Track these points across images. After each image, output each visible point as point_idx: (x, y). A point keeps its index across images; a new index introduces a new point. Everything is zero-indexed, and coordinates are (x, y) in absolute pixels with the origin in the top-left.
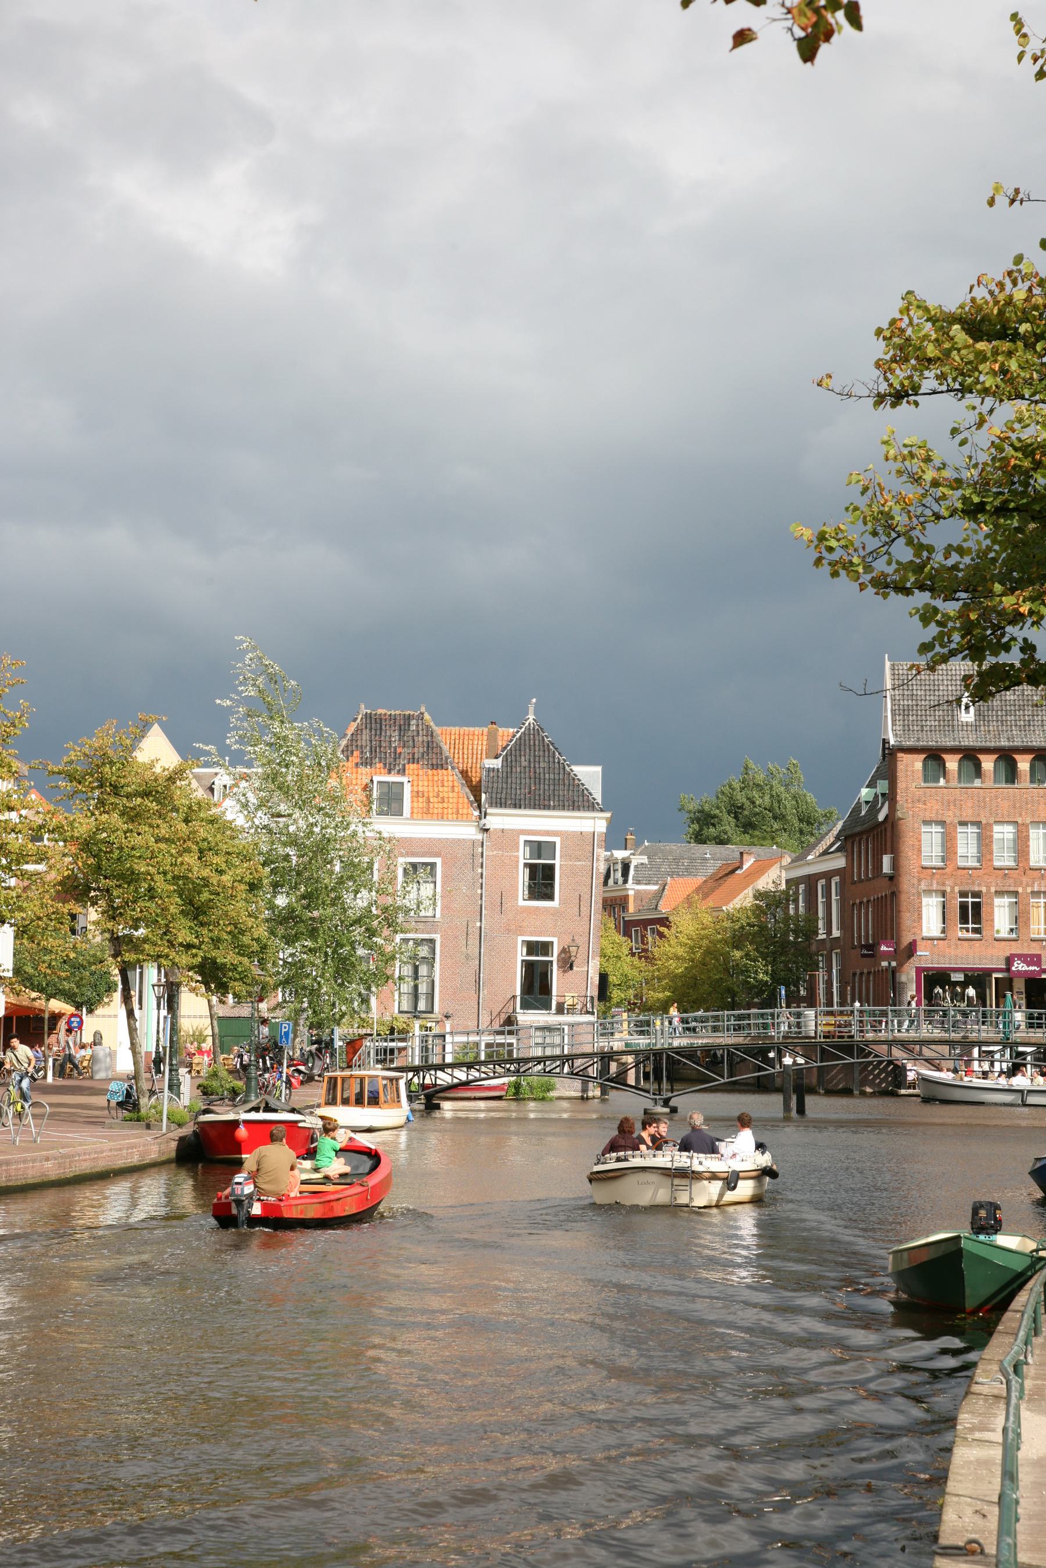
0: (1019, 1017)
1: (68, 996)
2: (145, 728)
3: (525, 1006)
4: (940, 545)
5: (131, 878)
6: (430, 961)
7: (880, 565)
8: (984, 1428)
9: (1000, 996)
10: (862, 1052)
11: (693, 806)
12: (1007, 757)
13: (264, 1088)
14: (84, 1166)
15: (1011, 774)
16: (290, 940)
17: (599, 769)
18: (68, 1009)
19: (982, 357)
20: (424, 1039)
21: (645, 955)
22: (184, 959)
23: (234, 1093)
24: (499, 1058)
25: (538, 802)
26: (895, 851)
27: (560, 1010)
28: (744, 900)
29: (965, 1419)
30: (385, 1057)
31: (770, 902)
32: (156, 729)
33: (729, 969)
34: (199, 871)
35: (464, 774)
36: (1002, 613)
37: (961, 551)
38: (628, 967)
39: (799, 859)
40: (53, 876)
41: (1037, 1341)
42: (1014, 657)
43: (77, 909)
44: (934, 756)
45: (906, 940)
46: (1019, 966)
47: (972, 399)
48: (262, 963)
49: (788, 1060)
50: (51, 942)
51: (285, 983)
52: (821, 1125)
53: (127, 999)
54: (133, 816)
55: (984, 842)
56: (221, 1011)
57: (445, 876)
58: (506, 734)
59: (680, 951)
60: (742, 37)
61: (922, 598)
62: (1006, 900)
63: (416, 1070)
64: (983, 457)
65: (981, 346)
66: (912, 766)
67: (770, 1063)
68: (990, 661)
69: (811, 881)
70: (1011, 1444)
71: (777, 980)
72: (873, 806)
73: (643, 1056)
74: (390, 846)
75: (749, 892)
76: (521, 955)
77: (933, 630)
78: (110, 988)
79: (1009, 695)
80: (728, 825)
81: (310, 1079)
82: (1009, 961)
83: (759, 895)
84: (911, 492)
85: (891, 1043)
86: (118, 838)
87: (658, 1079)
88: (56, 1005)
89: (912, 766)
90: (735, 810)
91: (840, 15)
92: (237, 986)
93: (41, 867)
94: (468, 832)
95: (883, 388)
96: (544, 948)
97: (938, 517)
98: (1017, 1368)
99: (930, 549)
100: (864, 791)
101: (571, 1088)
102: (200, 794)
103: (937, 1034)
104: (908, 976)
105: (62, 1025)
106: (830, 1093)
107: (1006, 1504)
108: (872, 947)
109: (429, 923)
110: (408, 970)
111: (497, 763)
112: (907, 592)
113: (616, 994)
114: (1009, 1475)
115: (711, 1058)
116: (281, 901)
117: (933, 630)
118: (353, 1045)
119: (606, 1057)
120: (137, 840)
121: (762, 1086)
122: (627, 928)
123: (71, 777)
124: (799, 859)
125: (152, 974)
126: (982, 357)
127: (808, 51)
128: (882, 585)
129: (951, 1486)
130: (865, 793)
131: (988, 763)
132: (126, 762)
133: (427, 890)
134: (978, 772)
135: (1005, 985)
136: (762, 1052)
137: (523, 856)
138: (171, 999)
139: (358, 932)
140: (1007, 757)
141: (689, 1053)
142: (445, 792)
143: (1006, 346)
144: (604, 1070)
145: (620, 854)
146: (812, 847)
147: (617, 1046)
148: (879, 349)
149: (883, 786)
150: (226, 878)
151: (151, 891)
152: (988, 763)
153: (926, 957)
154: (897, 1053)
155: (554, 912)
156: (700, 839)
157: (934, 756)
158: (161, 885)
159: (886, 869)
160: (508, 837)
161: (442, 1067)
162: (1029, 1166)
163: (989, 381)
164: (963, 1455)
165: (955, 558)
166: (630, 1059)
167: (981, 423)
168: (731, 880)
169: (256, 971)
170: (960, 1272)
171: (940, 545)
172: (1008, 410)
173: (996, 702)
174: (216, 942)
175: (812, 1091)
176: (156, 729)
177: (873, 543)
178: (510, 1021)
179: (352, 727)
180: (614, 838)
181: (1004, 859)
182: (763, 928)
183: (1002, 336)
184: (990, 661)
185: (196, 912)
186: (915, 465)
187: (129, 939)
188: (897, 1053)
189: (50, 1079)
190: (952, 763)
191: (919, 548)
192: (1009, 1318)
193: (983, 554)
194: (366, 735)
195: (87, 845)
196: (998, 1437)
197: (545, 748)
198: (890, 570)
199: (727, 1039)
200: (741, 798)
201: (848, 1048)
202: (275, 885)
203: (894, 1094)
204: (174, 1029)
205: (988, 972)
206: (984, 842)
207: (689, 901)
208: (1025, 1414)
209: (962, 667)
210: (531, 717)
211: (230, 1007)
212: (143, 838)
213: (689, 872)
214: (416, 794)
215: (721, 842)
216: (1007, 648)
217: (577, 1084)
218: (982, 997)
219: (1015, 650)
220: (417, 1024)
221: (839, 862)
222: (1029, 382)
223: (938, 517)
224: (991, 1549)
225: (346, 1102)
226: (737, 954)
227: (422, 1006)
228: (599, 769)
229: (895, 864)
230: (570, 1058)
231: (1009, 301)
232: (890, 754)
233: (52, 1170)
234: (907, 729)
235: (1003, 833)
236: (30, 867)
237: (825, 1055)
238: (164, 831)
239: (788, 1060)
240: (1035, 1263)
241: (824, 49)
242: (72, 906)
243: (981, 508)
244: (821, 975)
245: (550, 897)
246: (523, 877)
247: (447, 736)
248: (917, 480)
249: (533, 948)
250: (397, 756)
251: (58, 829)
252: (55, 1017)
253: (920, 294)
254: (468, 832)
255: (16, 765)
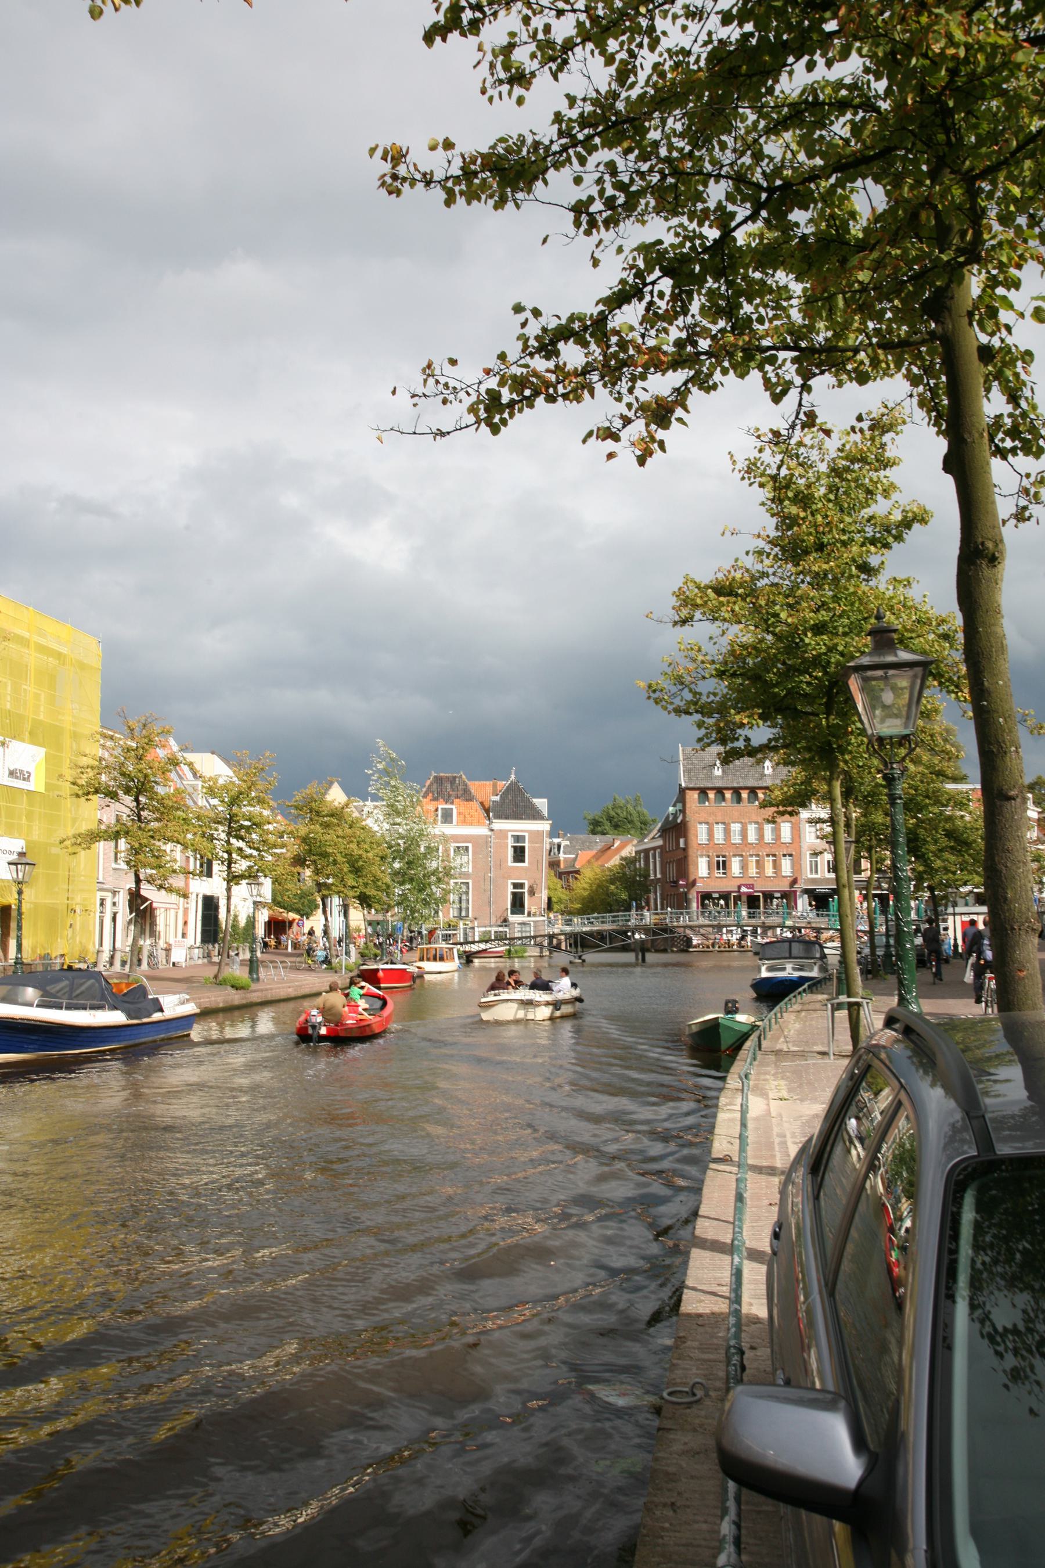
0: (744, 913)
1: (298, 911)
2: (331, 783)
3: (513, 913)
4: (704, 692)
5: (325, 855)
6: (467, 893)
7: (677, 702)
8: (730, 1104)
9: (735, 904)
10: (672, 932)
11: (590, 817)
12: (737, 791)
13: (390, 953)
14: (306, 991)
15: (739, 799)
16: (402, 883)
17: (545, 800)
18: (297, 917)
19: (722, 604)
20: (465, 930)
21: (569, 888)
22: (351, 893)
23: (376, 956)
24: (500, 937)
25: (517, 816)
26: (685, 836)
27: (529, 915)
28: (614, 861)
29: (723, 1101)
30: (447, 938)
31: (629, 862)
32: (336, 784)
33: (609, 894)
34: (357, 852)
35: (482, 803)
36: (734, 723)
37: (715, 695)
38: (562, 894)
39: (641, 841)
40: (289, 855)
41: (756, 1063)
42: (740, 744)
43: (301, 870)
44: (703, 792)
45: (691, 878)
46: (744, 889)
47: (718, 623)
48: (388, 895)
49: (637, 936)
50: (289, 886)
51: (399, 904)
52: (652, 966)
53: (324, 912)
54: (326, 826)
55: (727, 832)
56: (369, 918)
57: (474, 853)
58: (503, 785)
59: (586, 886)
60: (611, 456)
61: (697, 717)
62: (738, 859)
63: (461, 944)
64: (724, 650)
65: (722, 599)
66: (693, 796)
67: (629, 938)
68: (730, 745)
69: (646, 852)
70: (744, 1111)
71: (631, 899)
72: (675, 816)
73: (568, 936)
74: (446, 839)
75: (617, 857)
76: (510, 889)
77: (703, 731)
78: (317, 907)
79: (737, 762)
80: (607, 826)
81: (411, 949)
82: (739, 887)
83: (622, 859)
84: (691, 666)
85: (685, 927)
86: (319, 836)
87: (576, 946)
88: (292, 916)
89: (693, 796)
90: (610, 819)
91: (656, 445)
92: (377, 906)
93: (284, 851)
94: (483, 831)
95: (677, 618)
96: (521, 886)
97: (704, 678)
98: (746, 1076)
99: (700, 694)
100: (671, 809)
101: (535, 952)
102: (356, 814)
103: (707, 922)
104: (693, 895)
105: (295, 925)
106: (657, 951)
107: (742, 1138)
108: (676, 882)
109: (466, 875)
110: (457, 898)
111: (497, 798)
112: (691, 714)
113: (556, 907)
114: (744, 1125)
115: (601, 936)
116: (397, 865)
117: (703, 731)
118: (431, 932)
119: (551, 937)
120: (328, 837)
121: (625, 949)
122: (560, 875)
123: (297, 808)
124: (641, 841)
125: (336, 901)
126: (722, 604)
127: (642, 461)
128: (678, 711)
129: (717, 1131)
130: (671, 809)
131: (728, 795)
132: (322, 801)
133: (465, 859)
134: (724, 799)
135: (738, 898)
136: (625, 933)
137: (510, 842)
138: (345, 910)
139: (433, 878)
140: (737, 791)
141: (590, 934)
142: (473, 812)
143: (733, 599)
144: (550, 943)
145: (556, 840)
146: (645, 836)
147: (556, 931)
148: (674, 601)
149: (679, 806)
150: (370, 855)
151: (335, 862)
152: (728, 795)
153: (700, 886)
154: (688, 932)
155: (501, 864)
156: (594, 832)
157: (703, 792)
158: (339, 858)
159: (682, 845)
160: (503, 834)
161: (473, 942)
162: (750, 982)
163: (727, 615)
164: (722, 1117)
165: (712, 698)
166: (562, 937)
167: (724, 633)
168: (609, 852)
169: (385, 899)
170: (719, 1034)
171: (704, 692)
172: (736, 628)
173: (731, 765)
174: (366, 885)
175: (649, 950)
176: (336, 784)
177: (674, 689)
178: (505, 920)
179: (428, 783)
180: (552, 834)
181: (736, 839)
182: (624, 874)
183: (730, 594)
184: (730, 745)
185: (357, 871)
186: (693, 654)
187: (325, 884)
188: (688, 932)
189: (290, 950)
190: (711, 795)
191: (695, 693)
192: (742, 1054)
193: (724, 696)
194: (435, 786)
195: (305, 840)
196: (738, 1108)
197: (520, 790)
198: (682, 704)
199: (608, 927)
200: (612, 813)
201: (666, 930)
202: (394, 859)
203: (687, 951)
204: (347, 926)
205: (729, 893)
206: (727, 832)
207: (589, 862)
208: (750, 1097)
209: (717, 749)
210: (513, 777)
211: (373, 915)
212: (330, 836)
213: (589, 848)
214: (459, 814)
215: (604, 834)
216: (737, 739)
217: (538, 949)
218: (727, 905)
219: (741, 739)
220: (461, 923)
221: (660, 842)
222: (744, 616)
223: (704, 678)
224: (736, 1159)
225: (428, 960)
226: (612, 887)
227: (463, 914)
228: (545, 800)
229: (686, 843)
230: (535, 937)
231: (734, 579)
232: (682, 791)
233: (291, 992)
234: (690, 779)
235: (736, 827)
236: (278, 851)
237: (655, 933)
238: (340, 833)
239: (637, 936)
240: (754, 1028)
241: (649, 460)
242: (298, 869)
243: (723, 673)
244: (652, 896)
245: (523, 861)
246: (510, 852)
247: (474, 786)
248: (694, 660)
249: (516, 886)
250: (449, 796)
251: (291, 833)
252: (291, 923)
253: (692, 576)
254: (483, 831)
255: (272, 803)
